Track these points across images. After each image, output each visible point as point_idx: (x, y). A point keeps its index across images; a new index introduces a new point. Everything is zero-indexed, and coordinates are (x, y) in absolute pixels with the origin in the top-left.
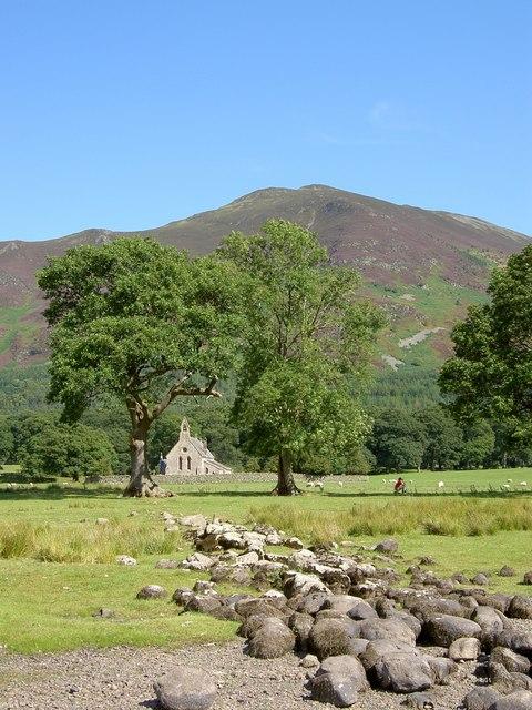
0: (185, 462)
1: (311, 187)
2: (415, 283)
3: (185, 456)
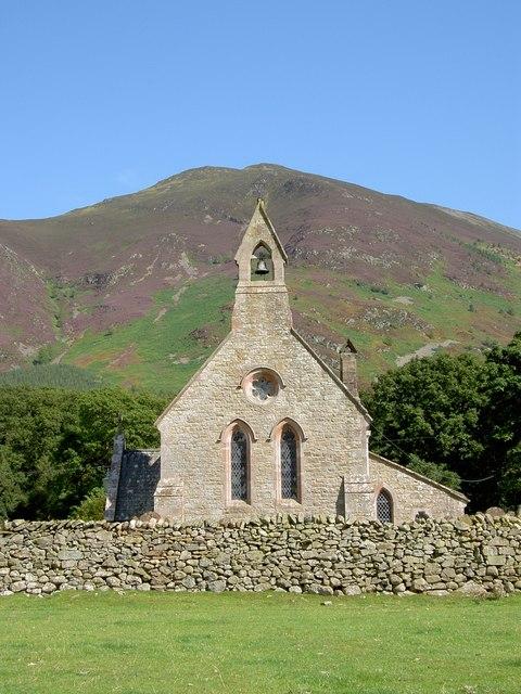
0: (268, 456)
1: (261, 165)
2: (412, 282)
3: (266, 415)
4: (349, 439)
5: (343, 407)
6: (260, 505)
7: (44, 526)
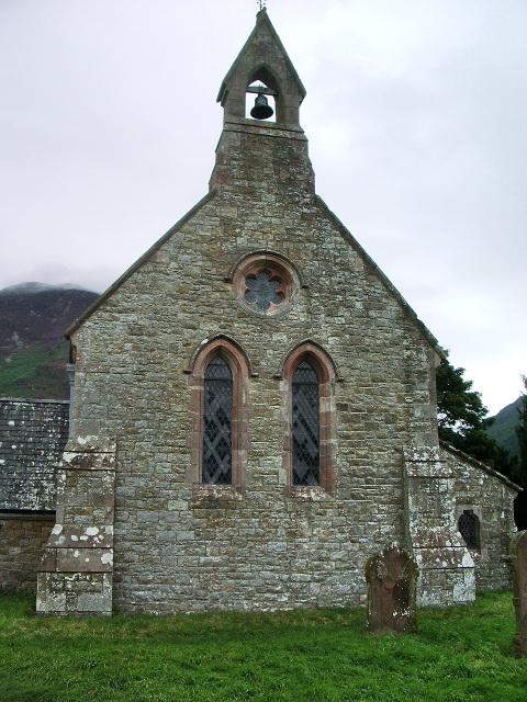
0: (266, 405)
5: (399, 332)
6: (259, 494)
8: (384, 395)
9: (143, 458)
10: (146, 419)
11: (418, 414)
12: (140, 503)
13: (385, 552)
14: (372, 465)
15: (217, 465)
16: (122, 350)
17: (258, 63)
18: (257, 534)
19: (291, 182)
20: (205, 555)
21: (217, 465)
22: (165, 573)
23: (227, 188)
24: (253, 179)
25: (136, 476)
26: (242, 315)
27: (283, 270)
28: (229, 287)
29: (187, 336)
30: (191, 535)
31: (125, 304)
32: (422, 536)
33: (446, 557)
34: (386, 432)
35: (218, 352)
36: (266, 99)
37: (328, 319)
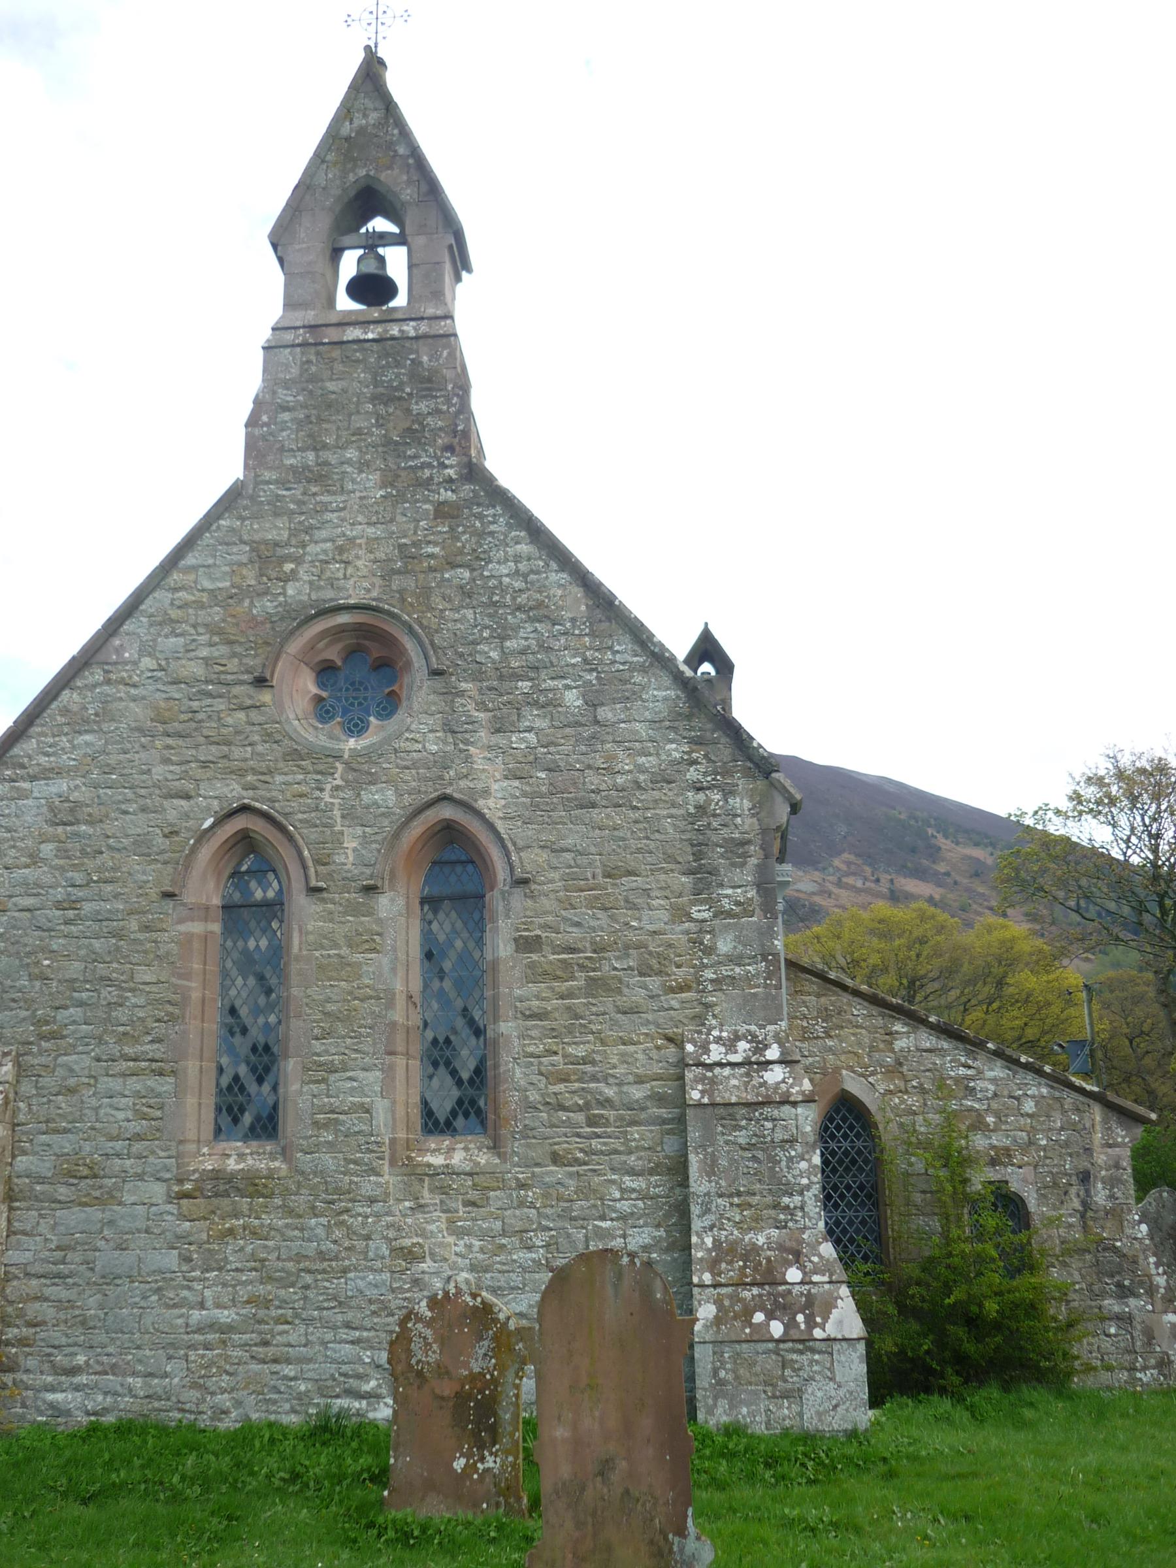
0: (363, 954)
4: (704, 879)
5: (675, 750)
6: (328, 1160)
7: (832, 902)
8: (634, 907)
9: (72, 1091)
10: (81, 1004)
11: (724, 946)
12: (63, 1192)
13: (433, 1302)
14: (605, 1079)
15: (248, 1105)
16: (35, 859)
17: (352, 178)
18: (322, 1256)
19: (415, 434)
20: (202, 1305)
21: (248, 1105)
22: (110, 1350)
23: (267, 475)
24: (325, 447)
25: (56, 1131)
26: (295, 755)
27: (387, 640)
28: (266, 697)
29: (172, 815)
30: (171, 1259)
31: (43, 760)
32: (724, 1252)
33: (780, 1307)
34: (637, 996)
35: (245, 842)
36: (382, 260)
37: (499, 739)
